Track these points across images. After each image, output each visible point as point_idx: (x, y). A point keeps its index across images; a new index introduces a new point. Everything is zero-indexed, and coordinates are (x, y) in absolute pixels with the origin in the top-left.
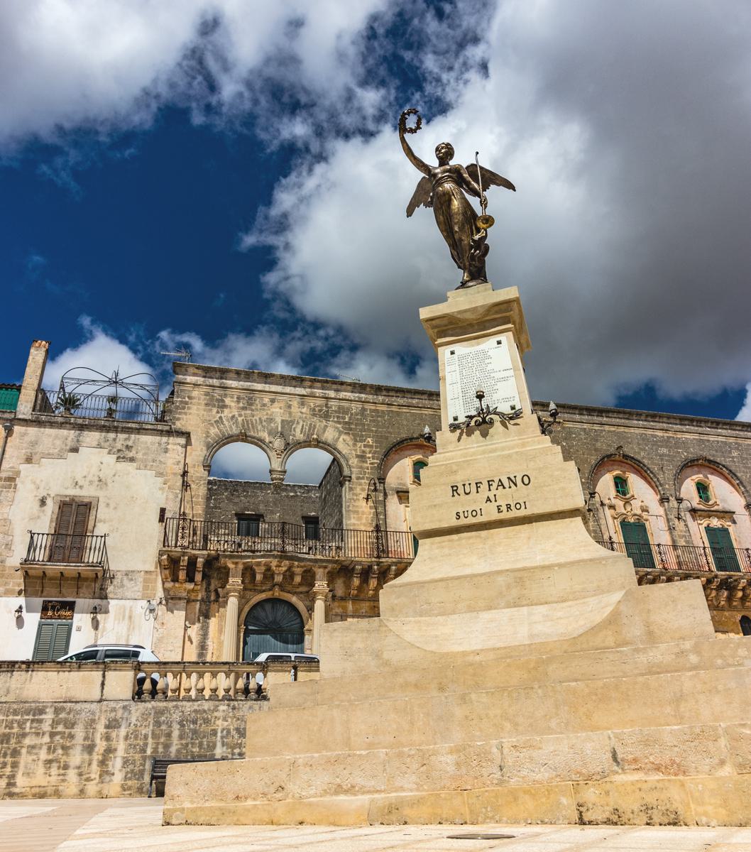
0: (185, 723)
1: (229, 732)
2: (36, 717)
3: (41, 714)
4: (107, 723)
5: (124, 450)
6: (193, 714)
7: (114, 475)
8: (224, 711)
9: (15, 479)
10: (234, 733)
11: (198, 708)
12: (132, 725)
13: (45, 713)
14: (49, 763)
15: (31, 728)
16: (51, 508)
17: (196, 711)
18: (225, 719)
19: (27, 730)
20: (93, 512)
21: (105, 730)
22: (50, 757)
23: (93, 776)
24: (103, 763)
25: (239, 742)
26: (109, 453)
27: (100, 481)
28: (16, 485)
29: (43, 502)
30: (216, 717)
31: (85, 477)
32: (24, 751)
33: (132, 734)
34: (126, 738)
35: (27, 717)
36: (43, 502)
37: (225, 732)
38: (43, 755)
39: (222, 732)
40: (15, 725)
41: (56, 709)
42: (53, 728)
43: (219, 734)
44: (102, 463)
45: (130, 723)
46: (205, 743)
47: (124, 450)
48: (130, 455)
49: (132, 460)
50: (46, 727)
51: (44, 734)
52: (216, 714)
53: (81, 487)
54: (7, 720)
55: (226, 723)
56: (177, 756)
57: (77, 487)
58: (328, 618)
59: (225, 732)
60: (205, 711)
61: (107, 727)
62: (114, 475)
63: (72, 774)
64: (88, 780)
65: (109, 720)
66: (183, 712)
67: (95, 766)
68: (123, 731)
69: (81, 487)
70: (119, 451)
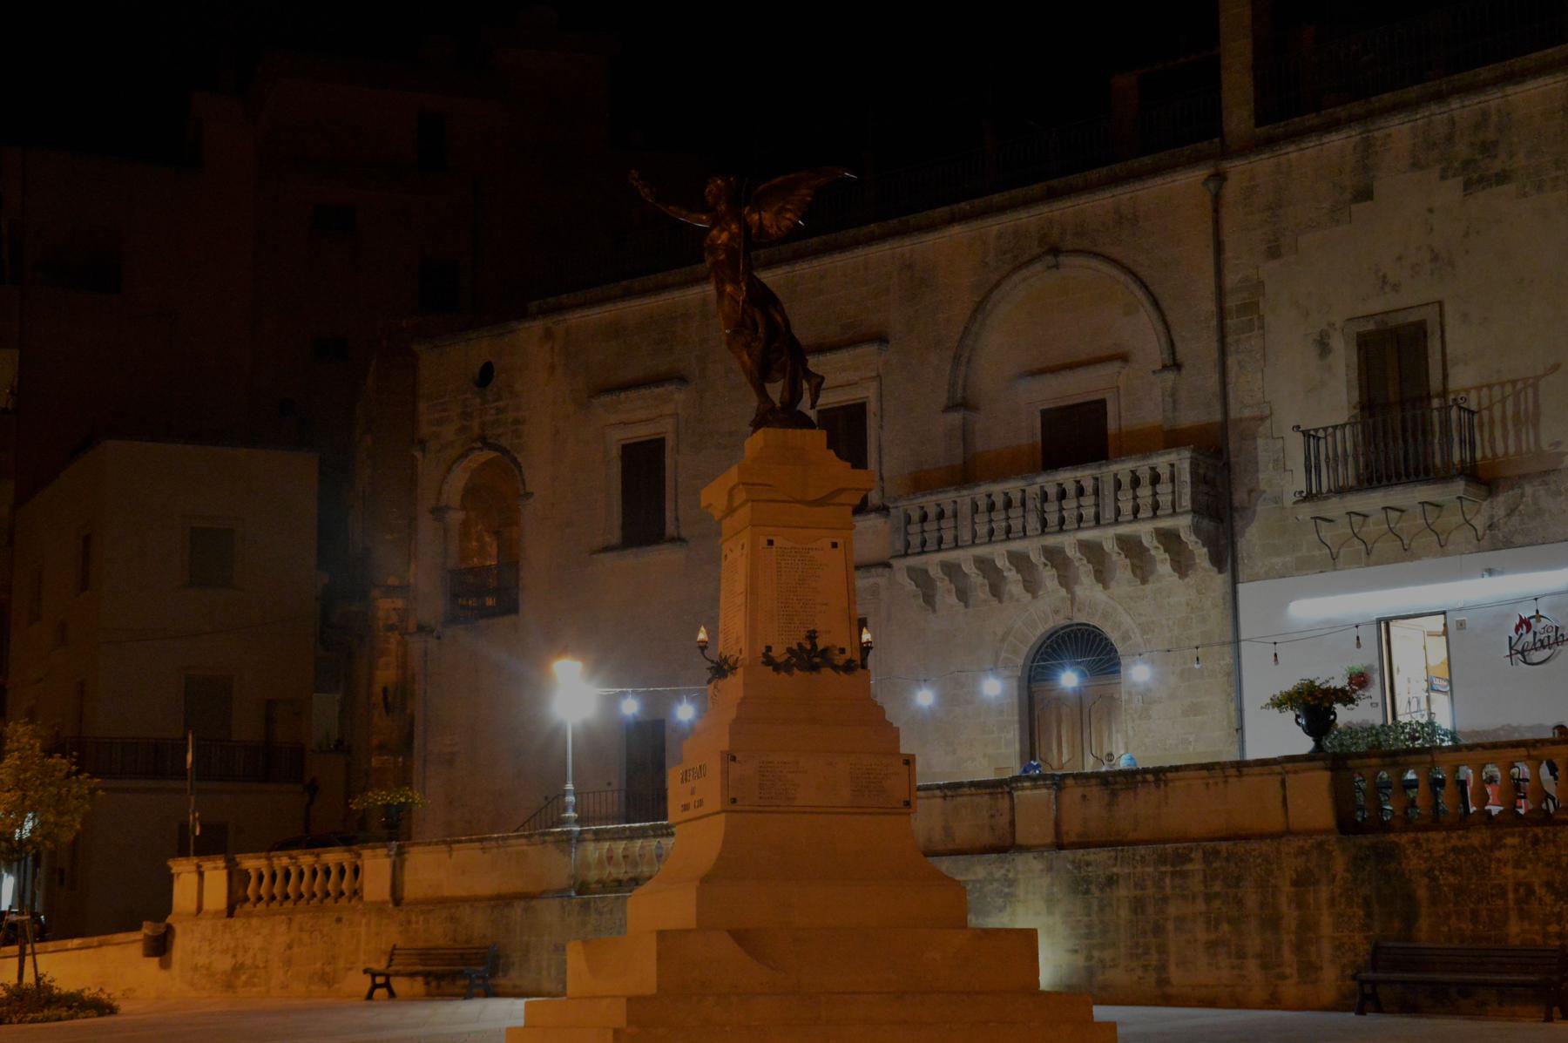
0: (1437, 873)
1: (1530, 891)
2: (1178, 869)
3: (1183, 863)
4: (1294, 876)
5: (1478, 157)
6: (1452, 856)
7: (1466, 235)
8: (1514, 847)
9: (1257, 304)
10: (1540, 891)
11: (1460, 844)
12: (1338, 878)
13: (1191, 860)
14: (1211, 946)
15: (1173, 887)
16: (1343, 356)
17: (1454, 849)
18: (1518, 864)
19: (1168, 890)
20: (1434, 345)
21: (1293, 889)
22: (1213, 936)
23: (1288, 971)
24: (1300, 947)
25: (1557, 909)
26: (1443, 177)
27: (1435, 258)
28: (1261, 318)
29: (1324, 347)
30: (1499, 861)
31: (1400, 258)
32: (1170, 926)
33: (1341, 895)
34: (1332, 902)
35: (1163, 869)
36: (1324, 347)
37: (1522, 890)
38: (1202, 935)
39: (1516, 890)
40: (1149, 883)
41: (1204, 853)
42: (1206, 887)
43: (1511, 896)
44: (1430, 211)
45: (1334, 877)
46: (1484, 913)
47: (1478, 157)
48: (1497, 166)
49: (1503, 178)
50: (1196, 884)
51: (1194, 898)
52: (1498, 854)
53: (1396, 288)
54: (1134, 874)
55: (1522, 873)
56: (359, 856)
57: (1387, 289)
58: (665, 818)
59: (1522, 890)
60: (1475, 849)
61: (1295, 883)
62: (1466, 235)
63: (1252, 967)
64: (1283, 977)
65: (1296, 870)
66: (1430, 851)
67: (1287, 954)
68: (1324, 892)
69: (1396, 288)
70: (1466, 164)
